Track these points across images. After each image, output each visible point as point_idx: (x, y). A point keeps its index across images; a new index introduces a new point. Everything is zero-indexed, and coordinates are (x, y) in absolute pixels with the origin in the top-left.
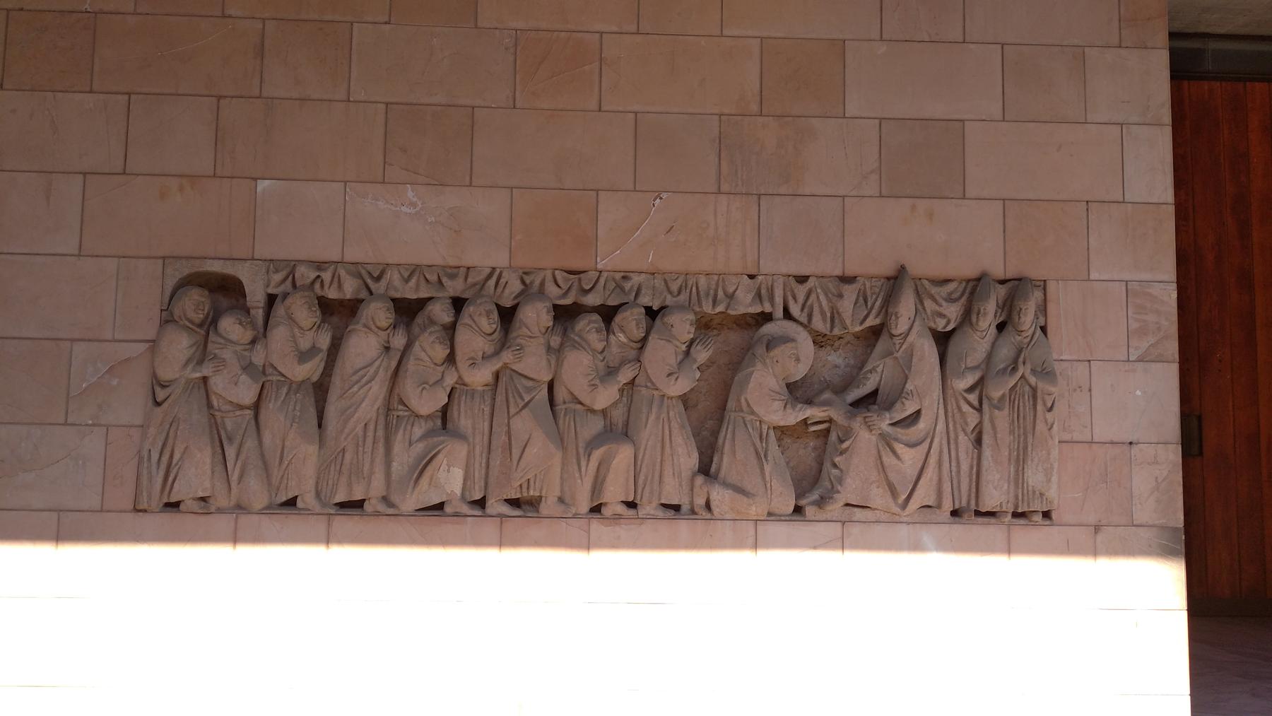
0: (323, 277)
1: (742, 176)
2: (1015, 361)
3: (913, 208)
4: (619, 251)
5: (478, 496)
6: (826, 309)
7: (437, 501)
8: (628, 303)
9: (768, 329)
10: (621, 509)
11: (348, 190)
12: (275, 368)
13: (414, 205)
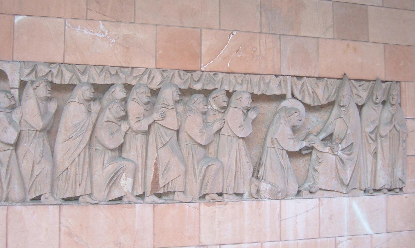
0: (54, 72)
1: (272, 25)
2: (392, 120)
3: (348, 45)
4: (212, 61)
5: (140, 192)
6: (310, 90)
7: (119, 196)
8: (217, 89)
9: (284, 103)
10: (216, 196)
11: (67, 23)
12: (28, 123)
13: (103, 33)
